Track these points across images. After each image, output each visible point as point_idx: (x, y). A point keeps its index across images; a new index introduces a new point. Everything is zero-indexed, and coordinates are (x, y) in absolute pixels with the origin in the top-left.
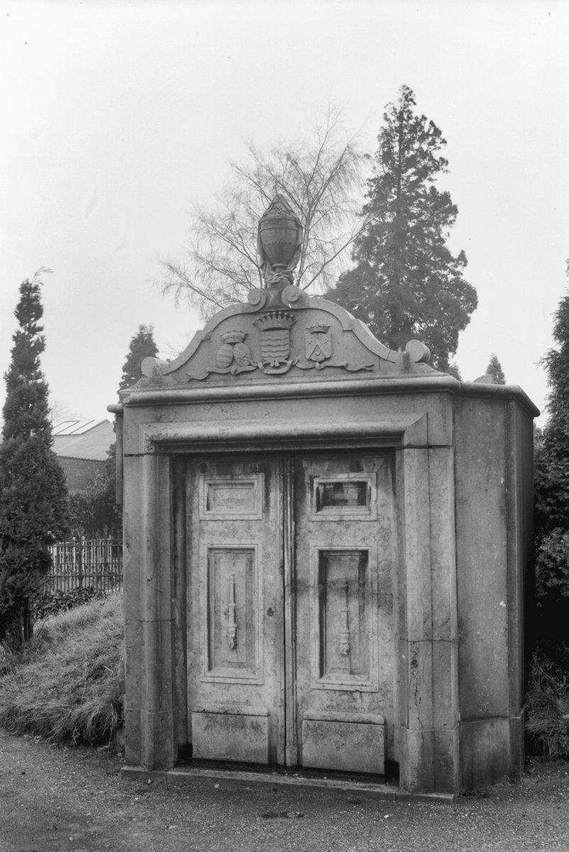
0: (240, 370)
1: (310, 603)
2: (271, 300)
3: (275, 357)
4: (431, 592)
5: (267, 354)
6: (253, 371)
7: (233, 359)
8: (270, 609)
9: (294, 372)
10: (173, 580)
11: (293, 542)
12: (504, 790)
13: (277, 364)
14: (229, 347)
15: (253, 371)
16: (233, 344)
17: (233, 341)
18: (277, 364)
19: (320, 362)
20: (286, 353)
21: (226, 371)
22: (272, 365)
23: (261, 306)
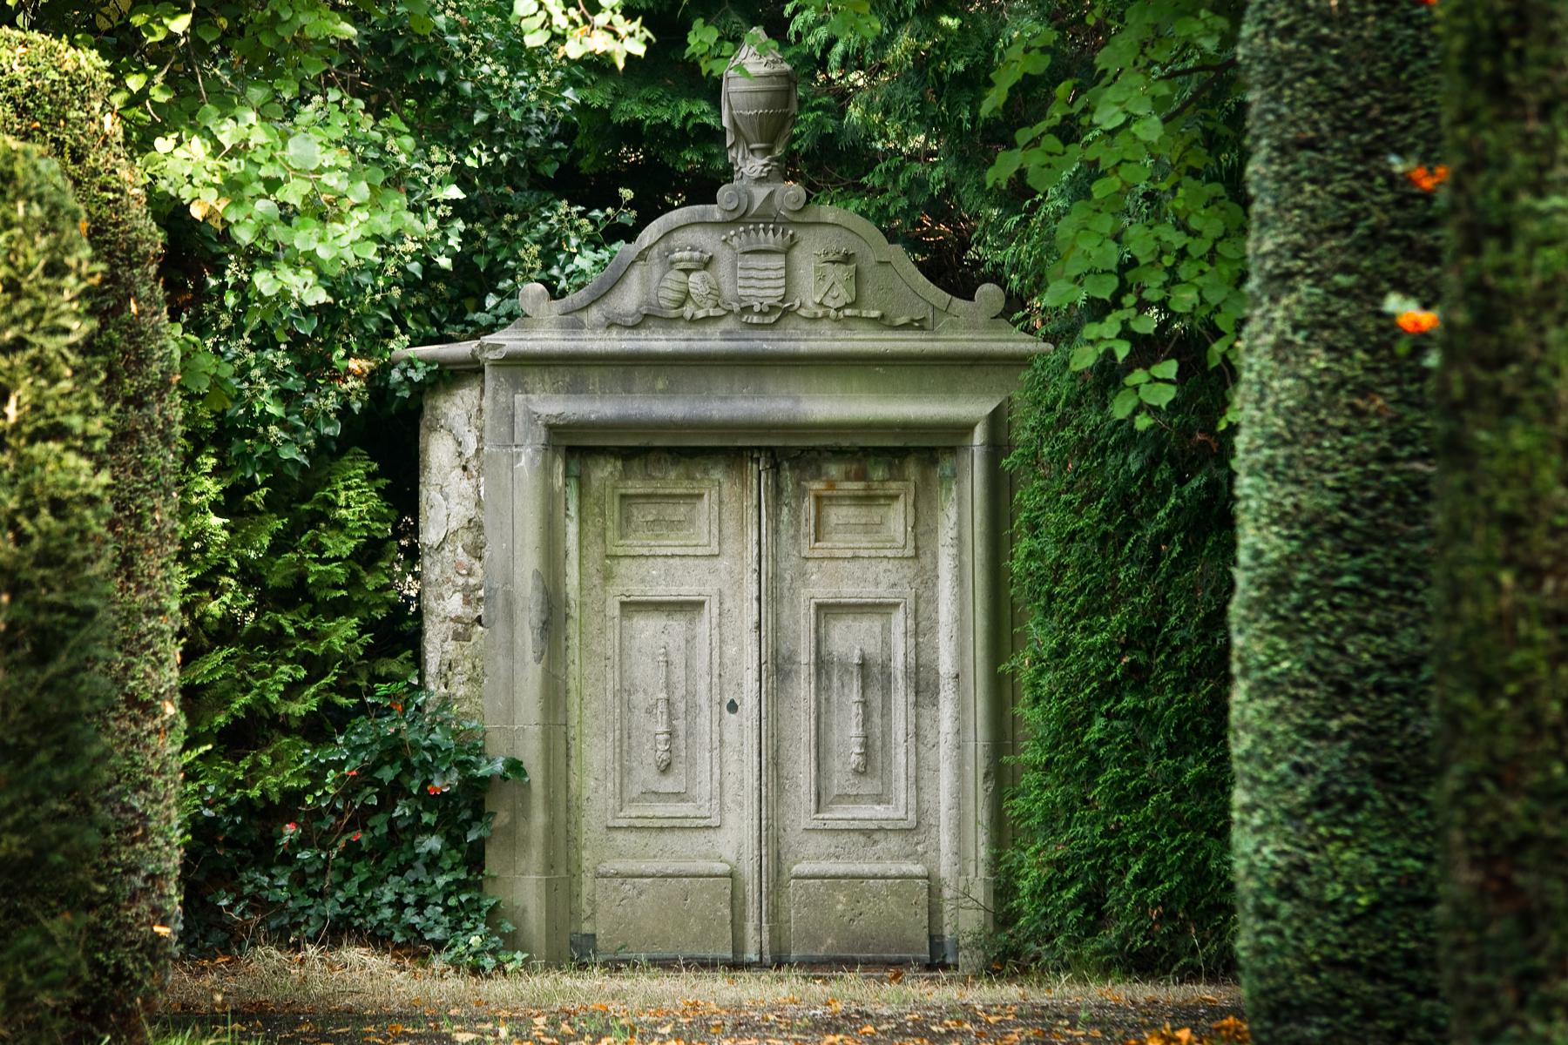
0: (700, 314)
1: (804, 688)
2: (757, 205)
3: (770, 292)
4: (796, 514)
5: (749, 292)
6: (720, 318)
7: (688, 294)
8: (732, 702)
9: (791, 322)
10: (594, 376)
11: (772, 595)
12: (1033, 849)
13: (766, 309)
14: (682, 276)
15: (720, 318)
16: (688, 272)
17: (689, 265)
18: (766, 309)
19: (838, 310)
20: (782, 291)
21: (673, 313)
22: (757, 309)
23: (736, 215)
